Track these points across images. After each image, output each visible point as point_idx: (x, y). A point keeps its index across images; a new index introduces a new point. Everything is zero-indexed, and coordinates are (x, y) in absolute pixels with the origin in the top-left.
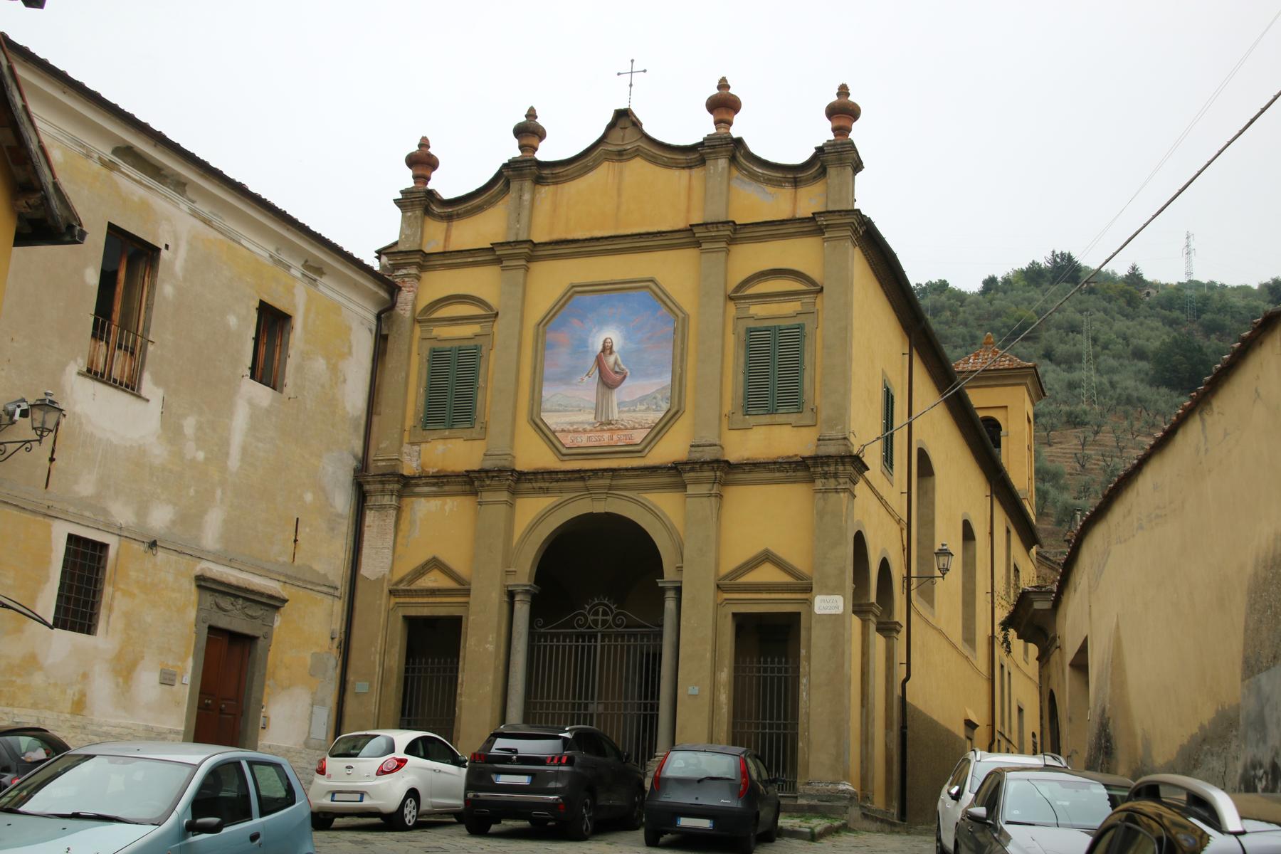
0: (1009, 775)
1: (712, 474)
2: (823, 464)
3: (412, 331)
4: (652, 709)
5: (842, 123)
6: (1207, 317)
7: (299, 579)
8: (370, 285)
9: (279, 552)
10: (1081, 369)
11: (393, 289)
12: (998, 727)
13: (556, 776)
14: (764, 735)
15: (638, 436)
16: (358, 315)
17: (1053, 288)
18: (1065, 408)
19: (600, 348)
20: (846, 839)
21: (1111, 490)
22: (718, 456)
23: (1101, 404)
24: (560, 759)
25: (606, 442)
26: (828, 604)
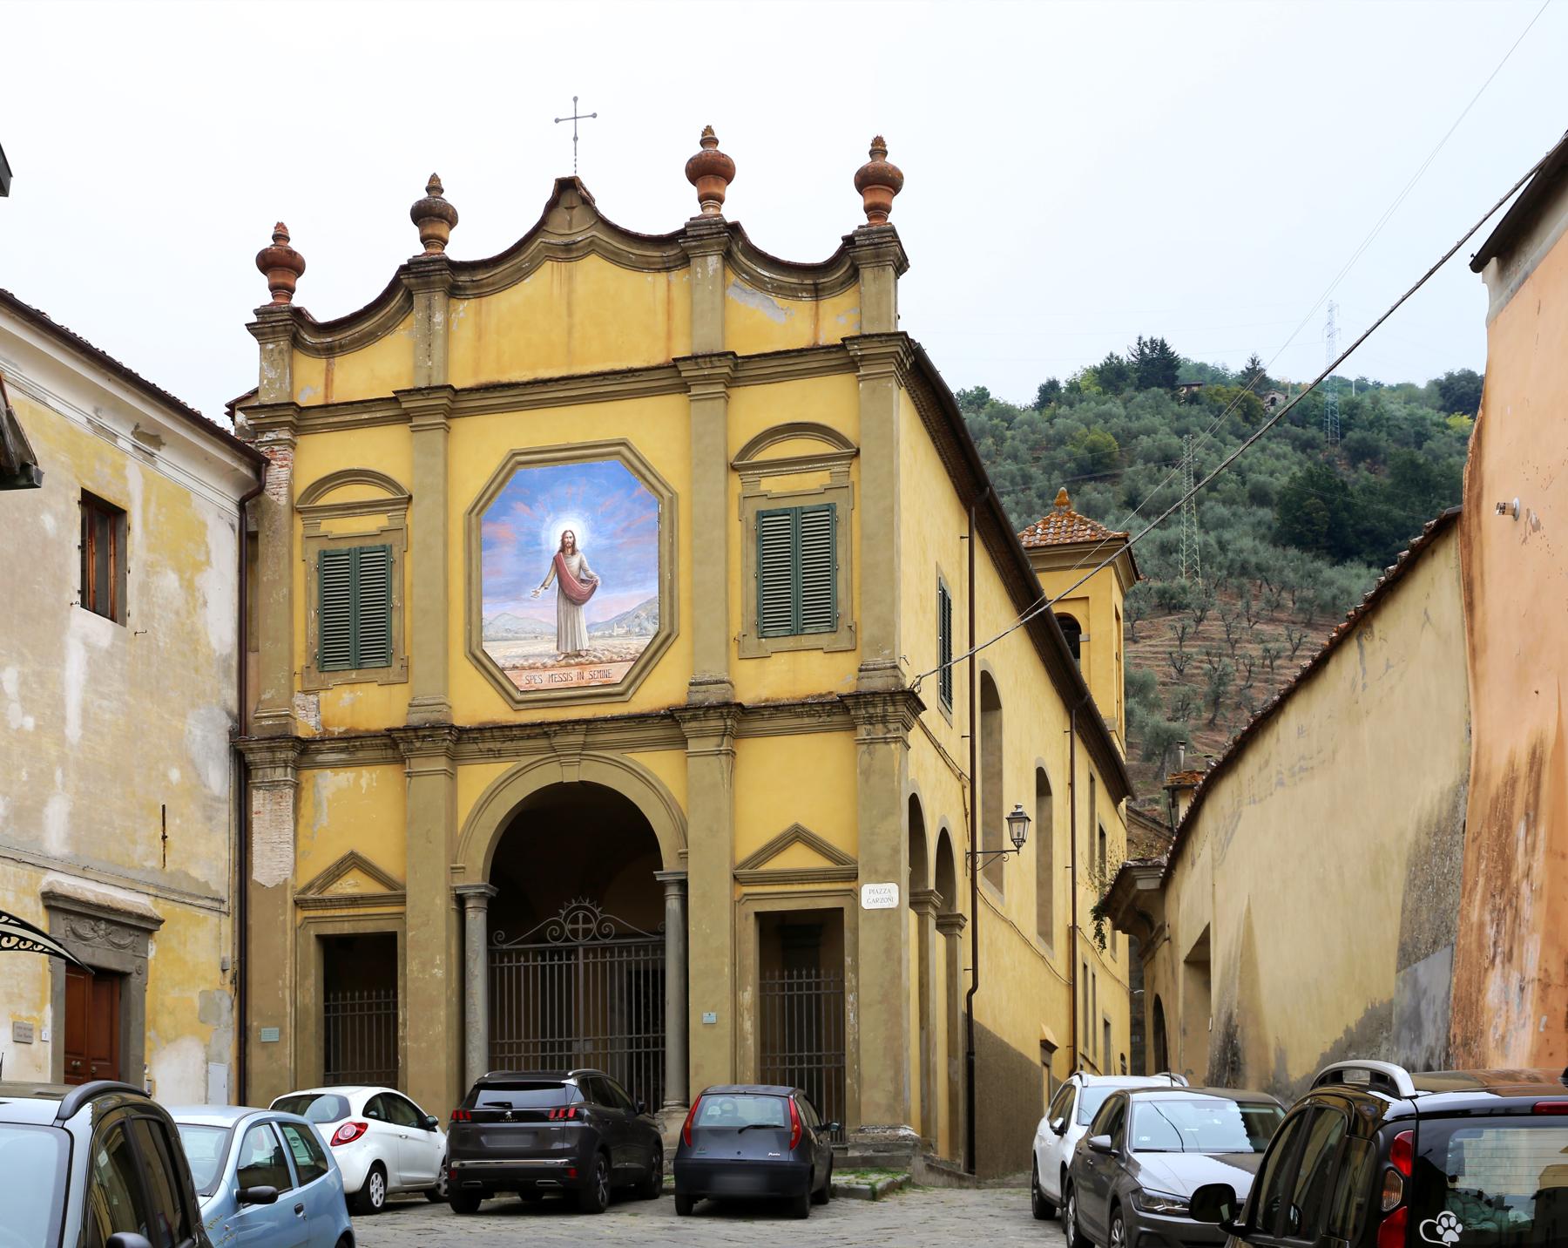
0: (1134, 1097)
1: (720, 723)
2: (866, 704)
3: (292, 527)
4: (656, 1045)
5: (879, 198)
6: (1354, 435)
7: (173, 891)
8: (226, 459)
9: (144, 853)
10: (1179, 522)
11: (259, 464)
12: (1080, 1048)
13: (563, 1134)
14: (801, 1071)
15: (618, 672)
16: (214, 504)
17: (1140, 397)
18: (1156, 584)
19: (558, 545)
20: (912, 1196)
21: (1245, 734)
22: (728, 697)
23: (1206, 576)
24: (566, 1112)
25: (574, 682)
26: (880, 896)
